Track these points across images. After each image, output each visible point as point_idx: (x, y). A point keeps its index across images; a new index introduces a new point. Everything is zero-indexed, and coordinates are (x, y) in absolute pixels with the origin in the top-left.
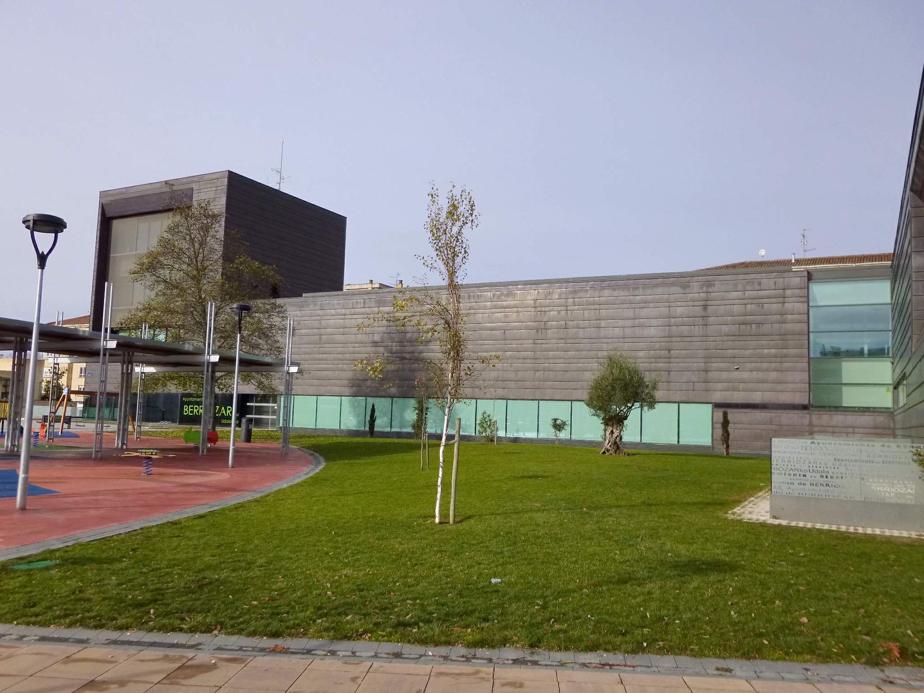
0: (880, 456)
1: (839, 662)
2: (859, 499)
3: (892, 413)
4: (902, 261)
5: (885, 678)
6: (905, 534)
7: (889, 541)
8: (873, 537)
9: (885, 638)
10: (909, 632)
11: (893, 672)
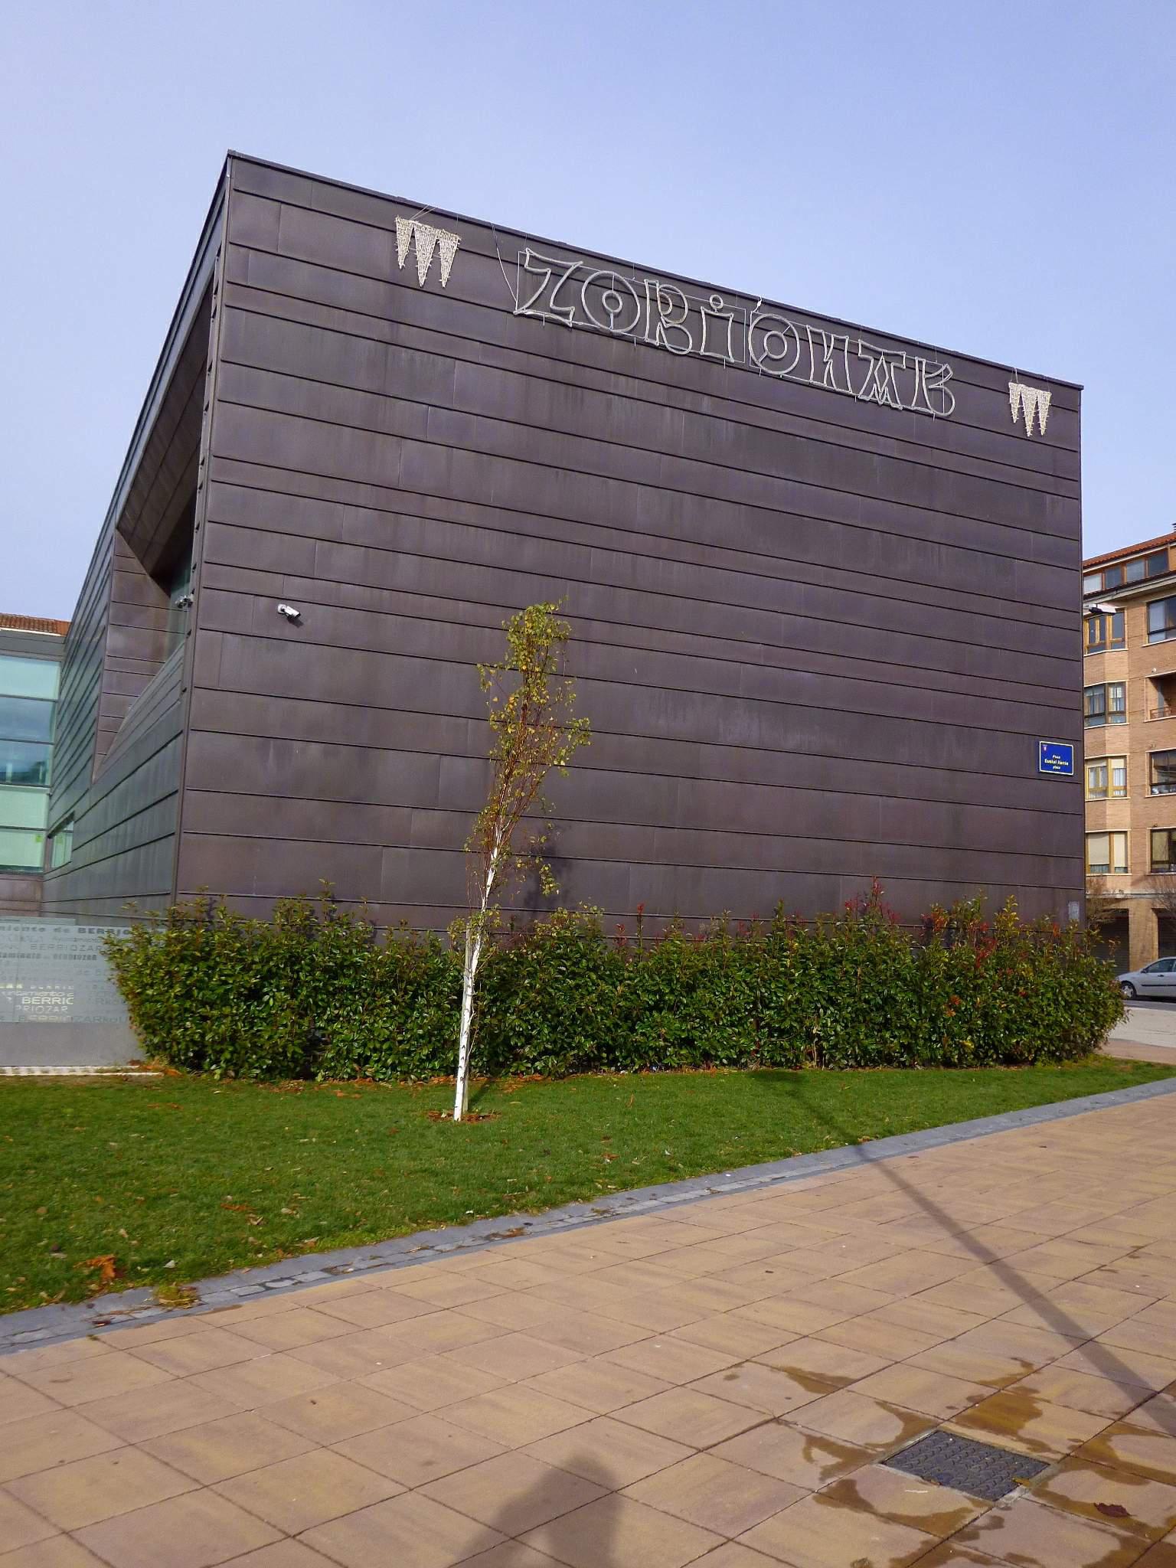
0: (52, 947)
1: (19, 1308)
2: (9, 1020)
3: (41, 876)
4: (88, 638)
5: (97, 1319)
6: (79, 1071)
7: (56, 1084)
8: (31, 1080)
9: (87, 1250)
10: (122, 1231)
11: (107, 1306)
